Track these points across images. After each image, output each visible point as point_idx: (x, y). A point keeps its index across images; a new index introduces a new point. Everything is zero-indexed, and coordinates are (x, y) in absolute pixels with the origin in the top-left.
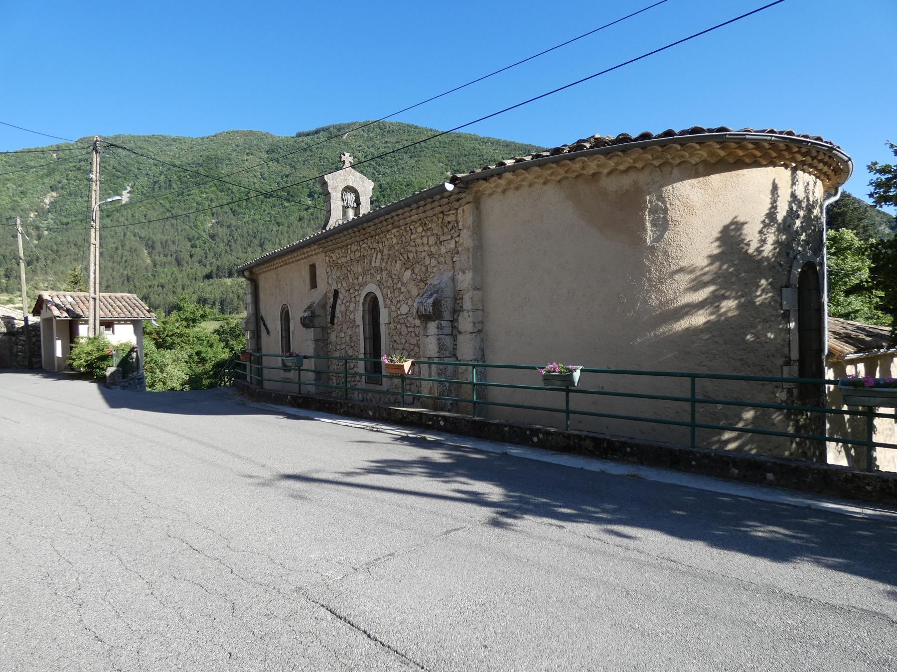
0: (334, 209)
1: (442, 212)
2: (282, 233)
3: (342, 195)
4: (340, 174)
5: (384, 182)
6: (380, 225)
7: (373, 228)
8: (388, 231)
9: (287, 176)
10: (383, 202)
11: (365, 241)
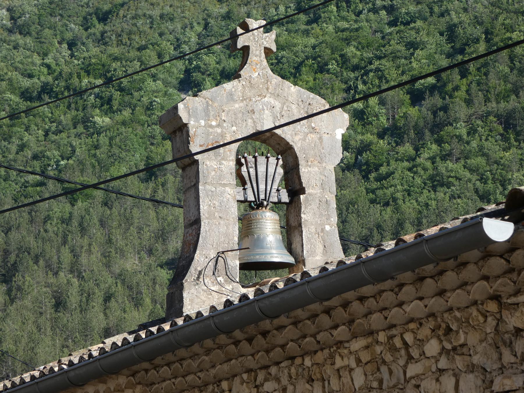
0: (211, 216)
1: (496, 298)
2: (83, 230)
3: (239, 163)
4: (231, 95)
5: (464, 17)
6: (310, 327)
7: (290, 332)
8: (340, 344)
9: (104, 18)
10: (462, 93)
11: (273, 370)
